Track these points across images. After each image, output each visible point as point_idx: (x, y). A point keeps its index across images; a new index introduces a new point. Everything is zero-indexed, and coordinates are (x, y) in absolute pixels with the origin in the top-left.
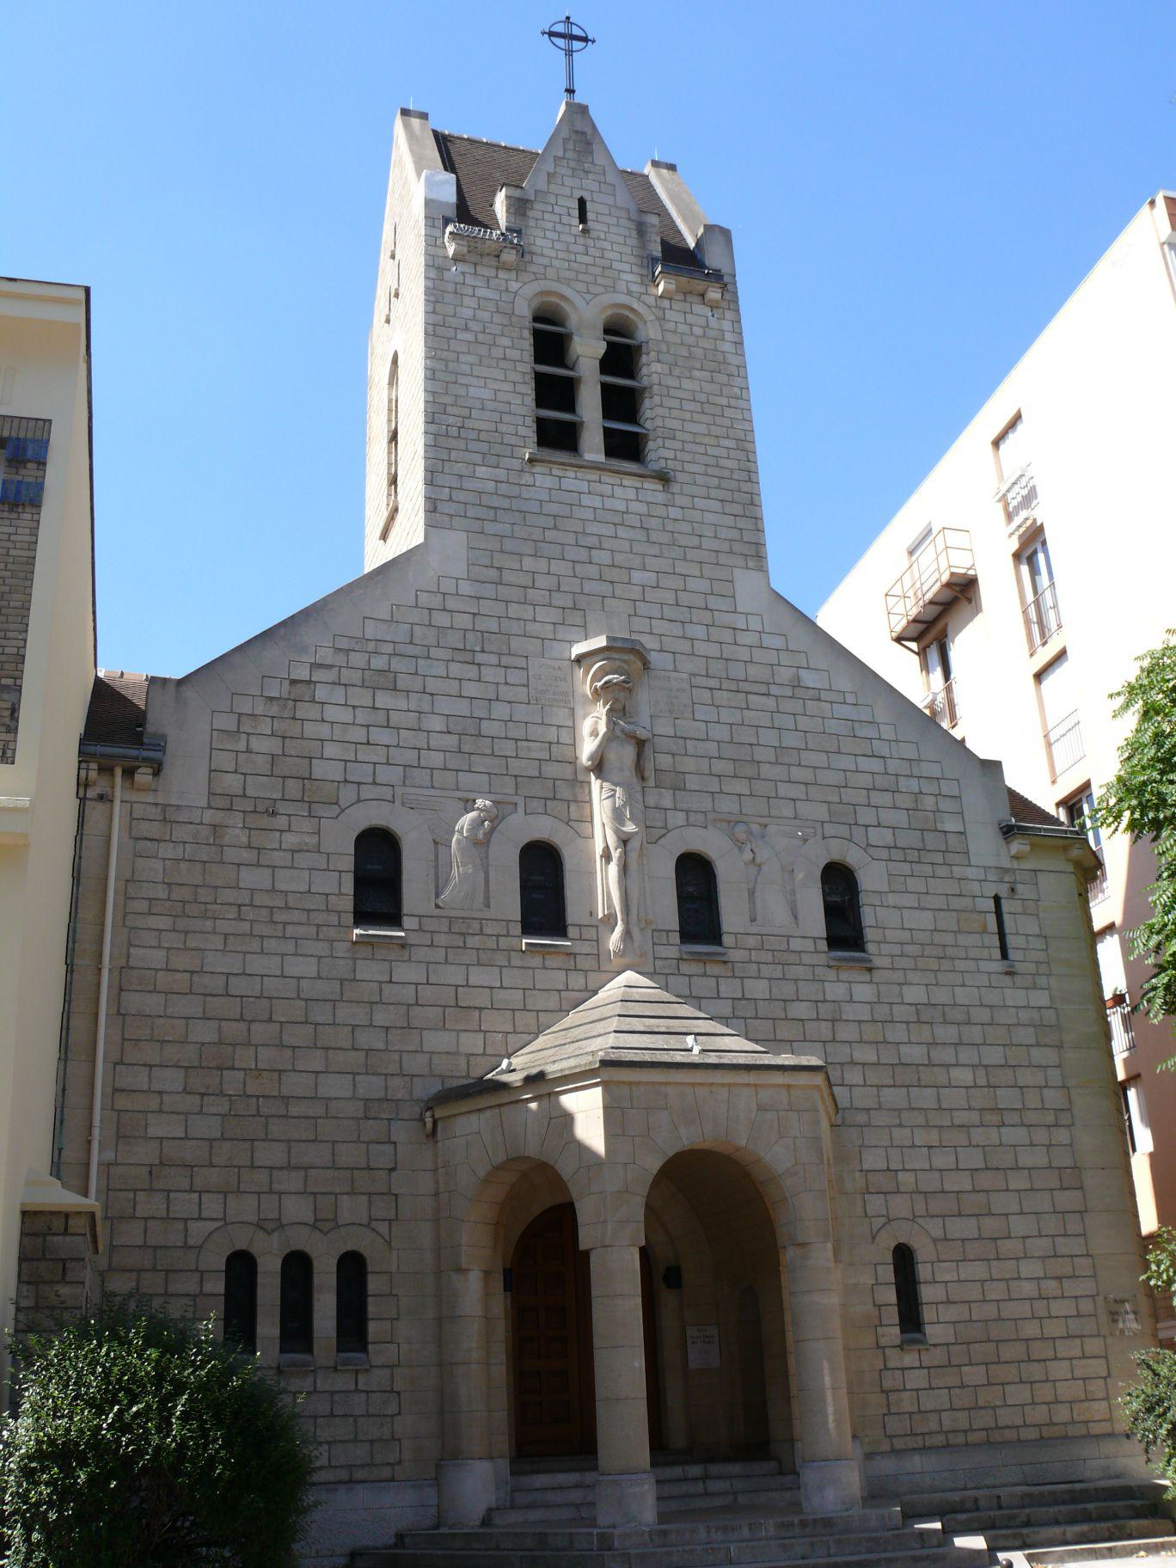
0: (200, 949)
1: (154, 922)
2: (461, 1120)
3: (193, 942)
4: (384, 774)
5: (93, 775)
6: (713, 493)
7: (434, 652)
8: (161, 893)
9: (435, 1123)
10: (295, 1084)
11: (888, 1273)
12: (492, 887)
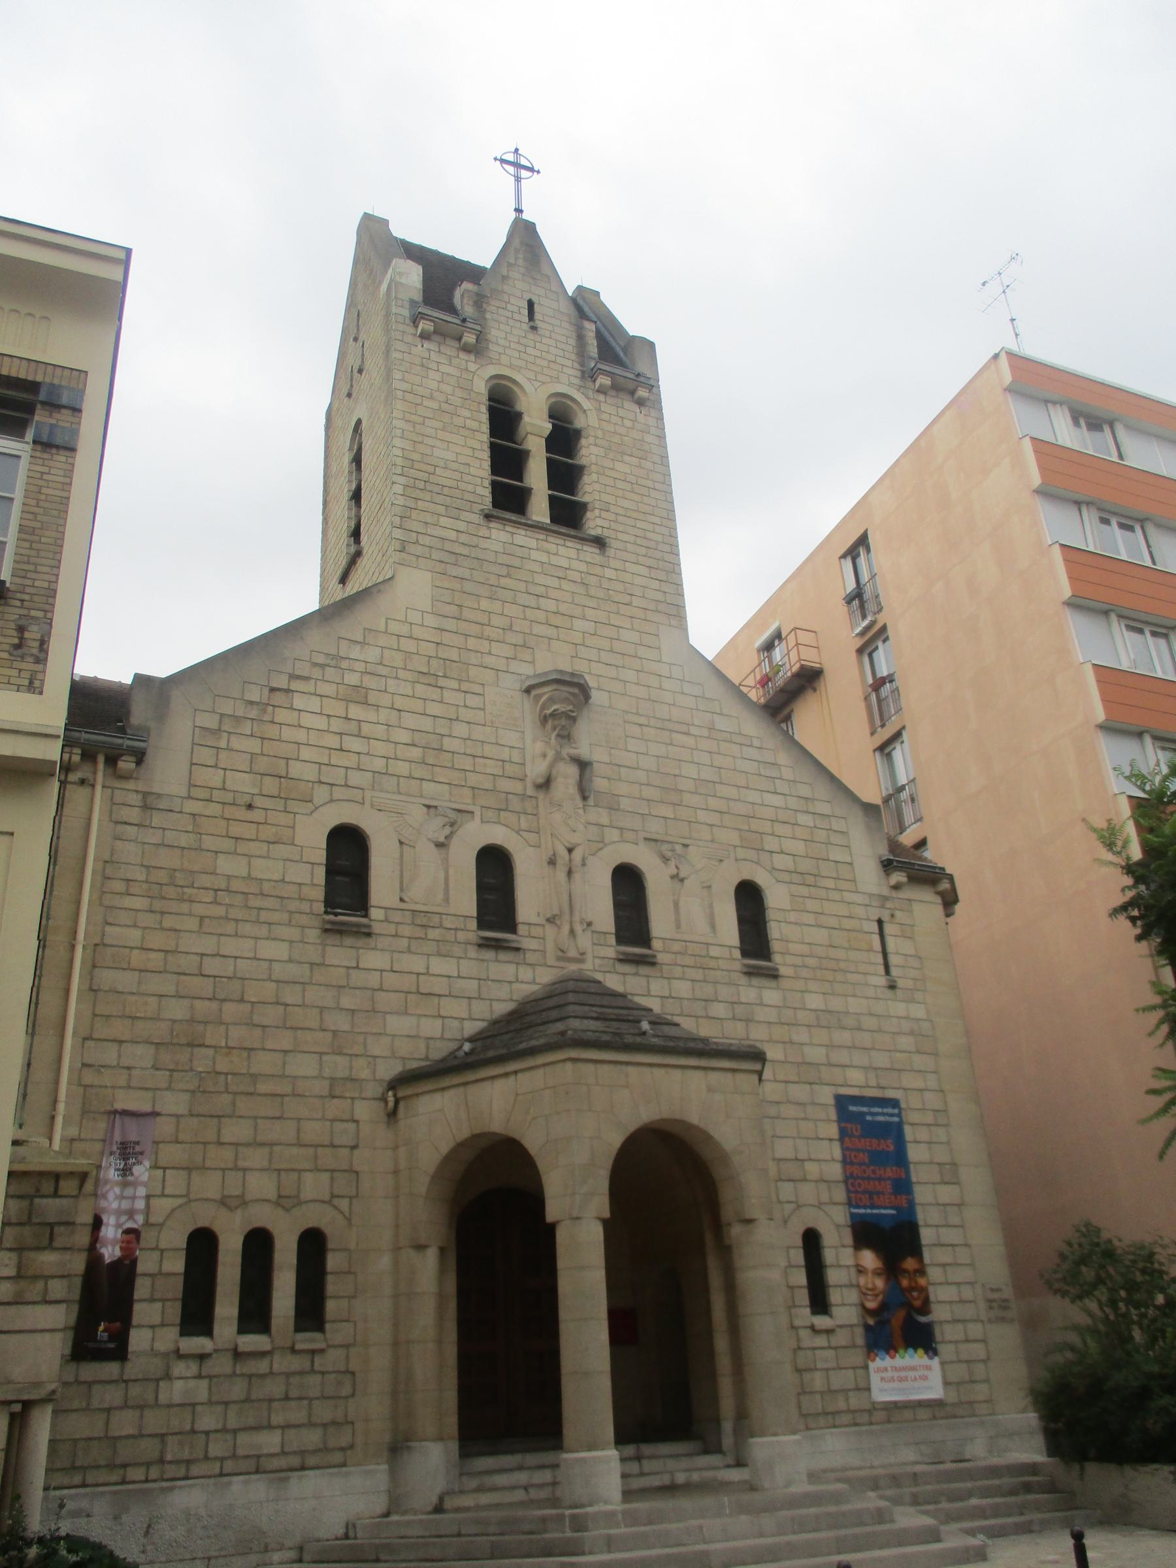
0: (176, 930)
1: (128, 902)
2: (424, 1099)
3: (168, 922)
4: (356, 778)
5: (76, 758)
6: (641, 560)
7: (401, 674)
8: (140, 875)
9: (397, 1102)
10: (263, 1063)
11: (798, 1257)
12: (452, 885)
